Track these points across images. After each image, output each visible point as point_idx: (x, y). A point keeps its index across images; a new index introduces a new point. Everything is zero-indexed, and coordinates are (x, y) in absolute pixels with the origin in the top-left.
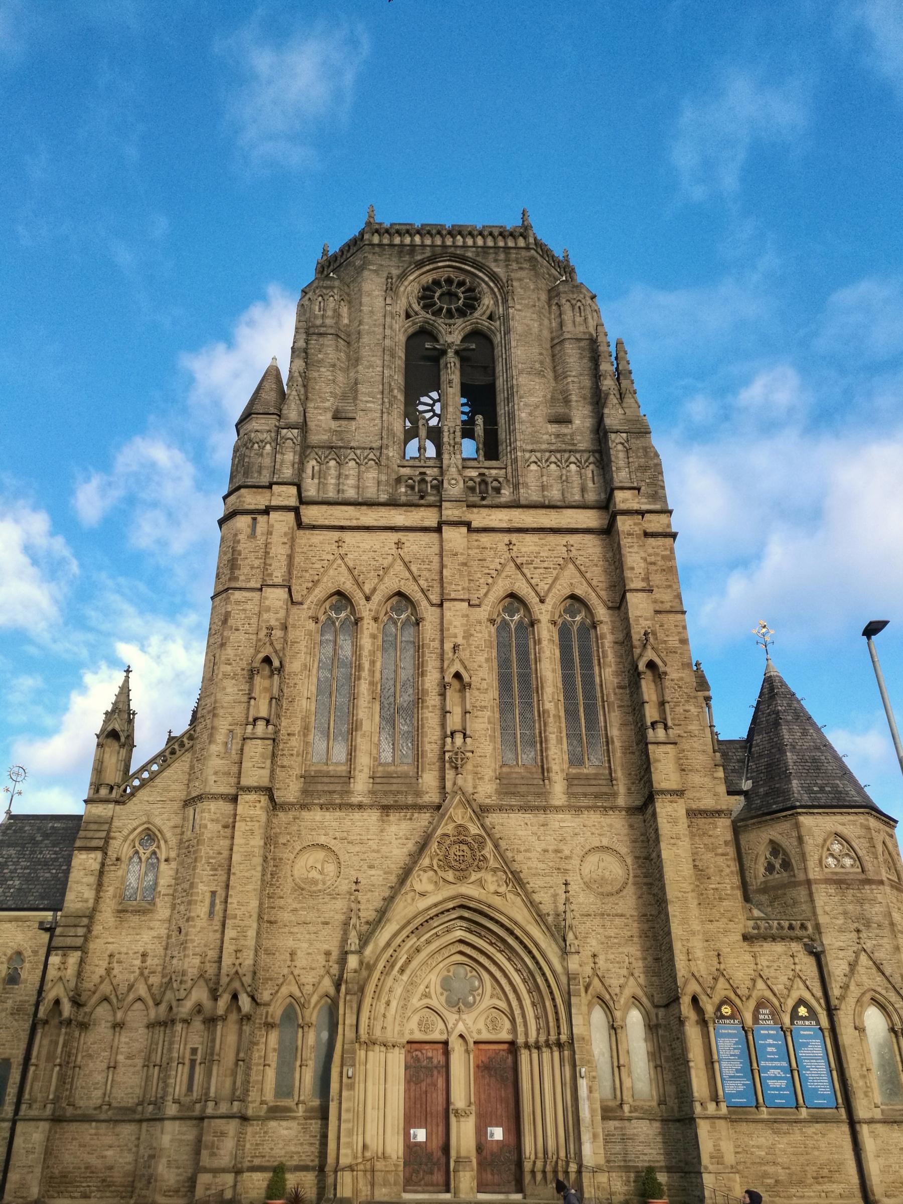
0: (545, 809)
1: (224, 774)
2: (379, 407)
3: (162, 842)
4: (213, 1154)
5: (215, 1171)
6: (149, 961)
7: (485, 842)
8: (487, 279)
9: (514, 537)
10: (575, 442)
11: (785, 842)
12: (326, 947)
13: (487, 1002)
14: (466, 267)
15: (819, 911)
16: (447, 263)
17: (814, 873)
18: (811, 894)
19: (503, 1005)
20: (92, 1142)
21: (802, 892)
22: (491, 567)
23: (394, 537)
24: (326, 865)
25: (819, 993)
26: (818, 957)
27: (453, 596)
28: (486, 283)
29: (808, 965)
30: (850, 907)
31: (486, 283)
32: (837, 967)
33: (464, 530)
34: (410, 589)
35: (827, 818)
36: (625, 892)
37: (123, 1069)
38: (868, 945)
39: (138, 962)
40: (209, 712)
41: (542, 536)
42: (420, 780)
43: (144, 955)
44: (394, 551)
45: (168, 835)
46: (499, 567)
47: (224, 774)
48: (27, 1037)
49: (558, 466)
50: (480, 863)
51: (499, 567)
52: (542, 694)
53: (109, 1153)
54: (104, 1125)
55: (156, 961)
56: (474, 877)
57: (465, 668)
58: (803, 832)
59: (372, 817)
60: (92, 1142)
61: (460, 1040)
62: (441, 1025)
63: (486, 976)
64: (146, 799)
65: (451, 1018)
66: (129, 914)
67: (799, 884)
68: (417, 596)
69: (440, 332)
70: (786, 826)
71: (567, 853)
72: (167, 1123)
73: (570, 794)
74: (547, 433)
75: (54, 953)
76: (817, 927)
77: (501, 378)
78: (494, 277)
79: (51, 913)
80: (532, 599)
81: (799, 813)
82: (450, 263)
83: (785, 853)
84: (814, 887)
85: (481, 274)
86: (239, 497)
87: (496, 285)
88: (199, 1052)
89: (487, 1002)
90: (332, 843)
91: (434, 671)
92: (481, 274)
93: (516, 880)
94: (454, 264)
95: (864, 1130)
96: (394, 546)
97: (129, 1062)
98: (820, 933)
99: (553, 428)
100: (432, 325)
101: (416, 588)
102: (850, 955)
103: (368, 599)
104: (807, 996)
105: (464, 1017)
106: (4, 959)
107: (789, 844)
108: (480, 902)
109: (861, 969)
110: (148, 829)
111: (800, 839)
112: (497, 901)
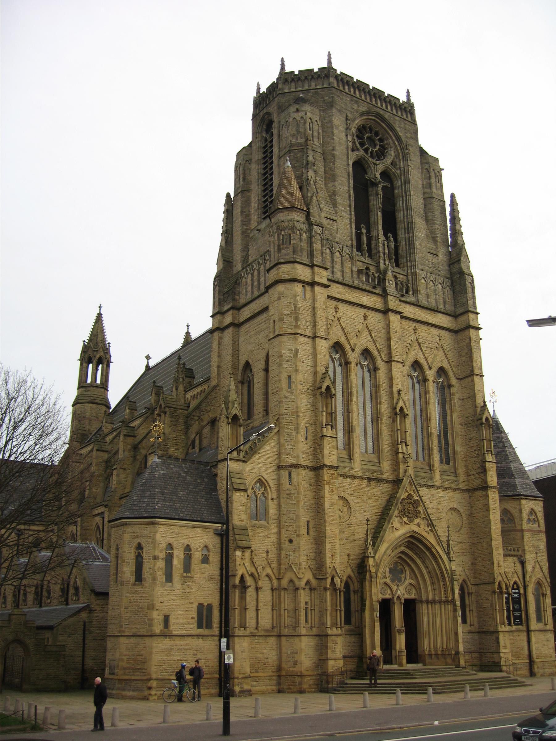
1: (306, 453)
6: (270, 555)
7: (419, 504)
8: (394, 138)
9: (417, 325)
12: (348, 552)
13: (408, 581)
14: (383, 125)
15: (525, 544)
16: (373, 118)
17: (525, 527)
18: (523, 536)
19: (413, 582)
23: (363, 311)
24: (343, 508)
25: (521, 579)
26: (523, 563)
27: (395, 359)
30: (535, 543)
31: (393, 140)
32: (529, 568)
33: (398, 316)
34: (372, 348)
35: (355, 442)
36: (462, 531)
37: (263, 610)
38: (539, 560)
39: (265, 555)
40: (292, 413)
41: (429, 327)
42: (381, 465)
43: (267, 552)
44: (363, 321)
46: (411, 343)
47: (306, 453)
50: (417, 514)
51: (411, 343)
52: (430, 423)
53: (265, 651)
54: (261, 638)
55: (273, 556)
56: (417, 521)
57: (405, 405)
58: (522, 507)
59: (365, 483)
61: (267, 579)
62: (389, 592)
63: (407, 569)
64: (257, 460)
65: (395, 588)
68: (375, 353)
69: (370, 167)
71: (441, 510)
74: (427, 260)
75: (238, 549)
76: (524, 550)
77: (402, 212)
78: (399, 139)
79: (221, 525)
80: (426, 367)
81: (521, 498)
82: (375, 118)
83: (511, 514)
84: (525, 533)
85: (391, 133)
86: (293, 268)
87: (399, 144)
89: (408, 581)
92: (391, 133)
93: (431, 525)
94: (377, 120)
96: (362, 318)
97: (264, 607)
98: (525, 554)
99: (429, 256)
100: (366, 161)
101: (375, 348)
103: (353, 350)
104: (518, 580)
105: (400, 587)
106: (199, 549)
107: (515, 512)
108: (419, 534)
110: (259, 479)
111: (520, 510)
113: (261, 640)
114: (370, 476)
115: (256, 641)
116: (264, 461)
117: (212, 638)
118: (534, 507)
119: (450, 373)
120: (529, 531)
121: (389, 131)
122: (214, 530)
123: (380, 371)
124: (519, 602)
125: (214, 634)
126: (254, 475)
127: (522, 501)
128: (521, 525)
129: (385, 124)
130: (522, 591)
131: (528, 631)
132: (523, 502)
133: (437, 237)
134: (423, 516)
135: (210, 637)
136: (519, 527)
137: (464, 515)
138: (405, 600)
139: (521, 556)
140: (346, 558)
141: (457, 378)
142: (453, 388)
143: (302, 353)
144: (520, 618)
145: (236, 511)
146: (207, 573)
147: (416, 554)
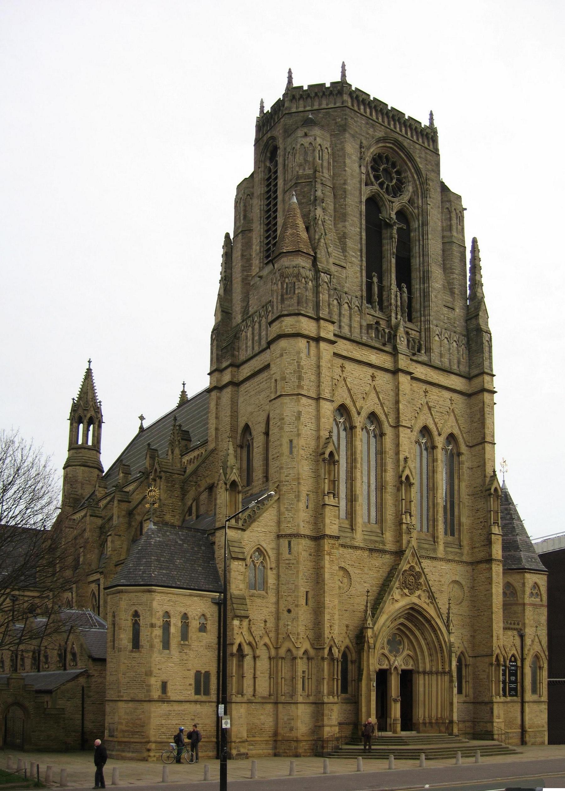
0: (435, 559)
2: (359, 262)
3: (267, 557)
4: (329, 719)
5: (331, 726)
6: (268, 624)
8: (413, 171)
9: (428, 387)
10: (456, 325)
11: (516, 584)
12: (347, 623)
13: (406, 652)
14: (402, 154)
15: (526, 618)
16: (391, 145)
17: (527, 601)
18: (524, 610)
20: (254, 712)
21: (520, 608)
22: (417, 406)
23: (371, 371)
25: (519, 652)
26: (522, 637)
28: (411, 173)
29: (518, 641)
31: (411, 173)
32: (528, 641)
39: (263, 625)
41: (440, 390)
42: (384, 536)
43: (265, 621)
44: (370, 382)
45: (270, 553)
47: (307, 522)
48: (216, 661)
49: (448, 341)
51: (420, 406)
53: (262, 717)
54: (258, 705)
56: (418, 593)
58: (526, 581)
59: (366, 553)
60: (254, 712)
62: (387, 662)
63: (406, 641)
65: (392, 659)
66: (256, 598)
67: (520, 604)
68: (382, 417)
70: (517, 577)
71: (443, 582)
72: (299, 705)
73: (446, 552)
78: (418, 171)
79: (218, 594)
81: (526, 572)
85: (410, 164)
87: (419, 178)
88: (307, 672)
89: (406, 652)
90: (347, 567)
91: (391, 470)
92: (410, 164)
94: (395, 148)
95: (526, 705)
96: (370, 378)
97: (262, 675)
98: (525, 627)
100: (381, 198)
101: (382, 412)
102: (532, 637)
103: (359, 414)
104: (516, 653)
105: (397, 658)
107: (518, 585)
108: (420, 606)
109: (535, 643)
110: (258, 548)
111: (524, 584)
112: (425, 606)
113: (258, 706)
114: (372, 546)
115: (253, 707)
116: (263, 530)
117: (210, 704)
118: (538, 581)
119: (461, 440)
120: (531, 604)
121: (408, 162)
122: (212, 599)
123: (387, 437)
124: (515, 675)
125: (211, 700)
126: (253, 544)
127: (526, 574)
128: (524, 598)
129: (404, 153)
130: (519, 664)
131: (523, 702)
132: (527, 576)
133: (455, 288)
134: (424, 588)
135: (207, 703)
136: (521, 601)
137: (466, 588)
138: (402, 671)
139: (521, 630)
140: (345, 628)
141: (467, 446)
142: (463, 456)
143: (305, 416)
144: (515, 689)
145: (234, 580)
146: (204, 641)
147: (415, 626)
